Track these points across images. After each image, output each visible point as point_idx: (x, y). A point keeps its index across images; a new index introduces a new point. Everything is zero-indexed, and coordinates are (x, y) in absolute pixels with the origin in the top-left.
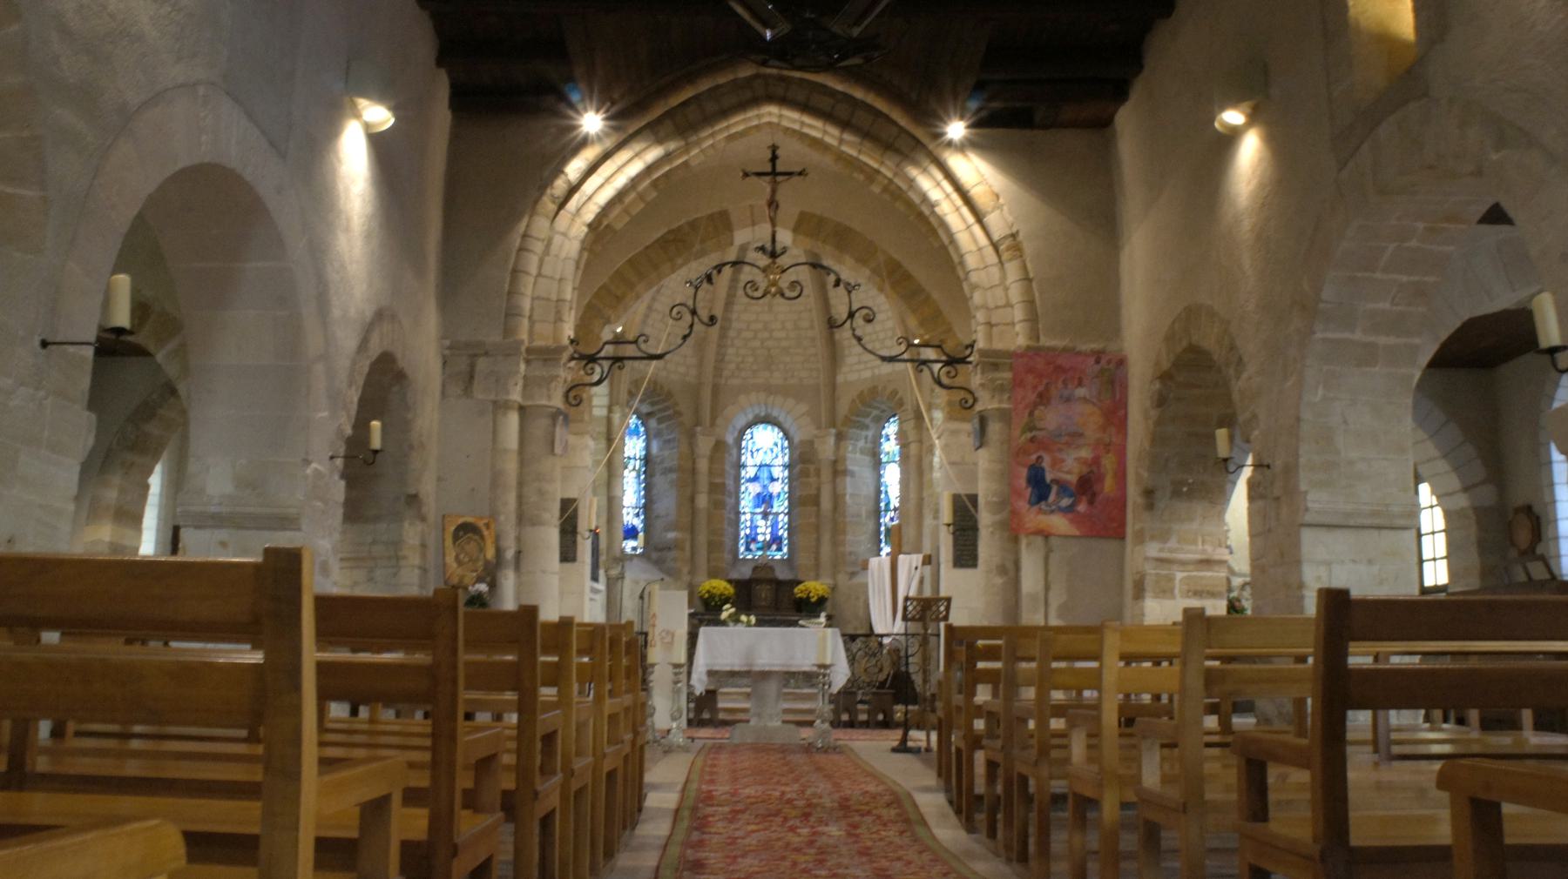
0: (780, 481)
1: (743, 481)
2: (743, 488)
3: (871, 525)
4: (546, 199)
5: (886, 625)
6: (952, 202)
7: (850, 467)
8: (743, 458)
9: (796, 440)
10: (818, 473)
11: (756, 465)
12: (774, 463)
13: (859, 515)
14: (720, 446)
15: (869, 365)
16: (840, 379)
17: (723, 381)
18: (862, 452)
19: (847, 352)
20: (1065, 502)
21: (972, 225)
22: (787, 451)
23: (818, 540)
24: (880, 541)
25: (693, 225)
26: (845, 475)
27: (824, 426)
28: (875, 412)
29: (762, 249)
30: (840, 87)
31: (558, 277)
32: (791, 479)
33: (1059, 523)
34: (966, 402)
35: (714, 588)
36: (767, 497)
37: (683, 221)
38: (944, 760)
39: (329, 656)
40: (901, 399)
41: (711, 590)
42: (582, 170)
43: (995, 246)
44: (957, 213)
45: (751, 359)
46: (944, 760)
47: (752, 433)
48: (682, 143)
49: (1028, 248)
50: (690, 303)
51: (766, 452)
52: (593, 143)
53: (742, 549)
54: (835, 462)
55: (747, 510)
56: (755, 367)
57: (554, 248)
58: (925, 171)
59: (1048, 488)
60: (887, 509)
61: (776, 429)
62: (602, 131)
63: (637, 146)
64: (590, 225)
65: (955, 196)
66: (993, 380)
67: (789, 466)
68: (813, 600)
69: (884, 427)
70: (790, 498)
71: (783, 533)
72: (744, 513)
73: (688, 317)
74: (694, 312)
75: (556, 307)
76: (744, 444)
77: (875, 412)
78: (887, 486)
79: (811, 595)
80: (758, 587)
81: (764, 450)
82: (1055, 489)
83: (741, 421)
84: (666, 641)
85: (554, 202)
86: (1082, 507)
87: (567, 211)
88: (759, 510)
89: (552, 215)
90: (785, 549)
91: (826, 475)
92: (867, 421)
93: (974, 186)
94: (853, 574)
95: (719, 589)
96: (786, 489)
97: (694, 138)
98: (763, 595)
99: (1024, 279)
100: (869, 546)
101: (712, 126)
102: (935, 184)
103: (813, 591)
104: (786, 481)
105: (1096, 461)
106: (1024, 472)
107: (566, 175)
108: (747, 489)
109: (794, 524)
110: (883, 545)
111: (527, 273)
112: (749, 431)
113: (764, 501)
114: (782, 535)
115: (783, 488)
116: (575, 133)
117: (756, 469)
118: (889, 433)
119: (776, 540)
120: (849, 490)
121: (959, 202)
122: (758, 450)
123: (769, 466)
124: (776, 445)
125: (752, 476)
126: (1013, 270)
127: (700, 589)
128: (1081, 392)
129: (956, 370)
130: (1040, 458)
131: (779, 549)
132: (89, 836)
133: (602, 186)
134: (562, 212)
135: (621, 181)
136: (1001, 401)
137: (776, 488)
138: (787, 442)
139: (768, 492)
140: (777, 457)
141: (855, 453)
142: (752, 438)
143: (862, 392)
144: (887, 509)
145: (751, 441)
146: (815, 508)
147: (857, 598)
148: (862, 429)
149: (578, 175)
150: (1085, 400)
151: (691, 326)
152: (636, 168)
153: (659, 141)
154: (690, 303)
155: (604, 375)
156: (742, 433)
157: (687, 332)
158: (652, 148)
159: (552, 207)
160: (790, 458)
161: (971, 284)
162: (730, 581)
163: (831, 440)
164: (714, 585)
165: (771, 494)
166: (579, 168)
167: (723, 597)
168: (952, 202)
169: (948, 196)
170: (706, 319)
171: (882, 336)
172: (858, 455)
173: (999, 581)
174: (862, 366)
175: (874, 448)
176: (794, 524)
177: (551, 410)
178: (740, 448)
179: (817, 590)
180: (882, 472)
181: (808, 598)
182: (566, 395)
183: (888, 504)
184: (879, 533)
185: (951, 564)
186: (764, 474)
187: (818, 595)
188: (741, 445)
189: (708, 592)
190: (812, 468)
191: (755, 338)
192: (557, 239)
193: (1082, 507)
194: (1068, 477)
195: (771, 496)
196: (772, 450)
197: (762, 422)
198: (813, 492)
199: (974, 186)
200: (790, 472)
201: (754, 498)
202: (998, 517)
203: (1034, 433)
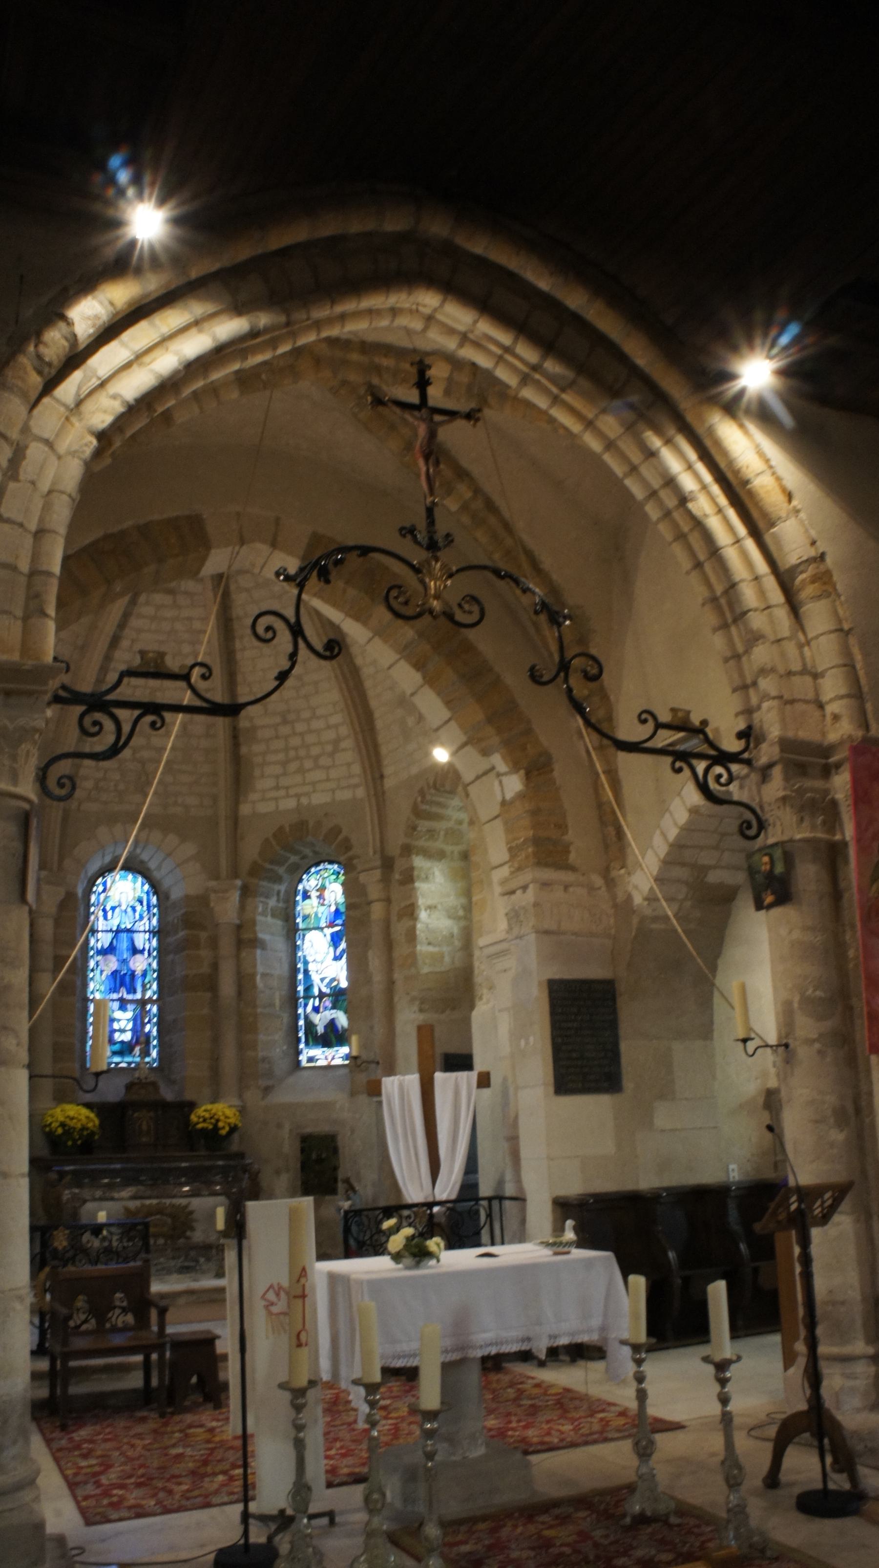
0: (146, 953)
1: (91, 953)
2: (92, 964)
3: (286, 1018)
4: (25, 361)
5: (422, 1186)
6: (713, 499)
7: (261, 935)
9: (176, 894)
10: (214, 943)
11: (111, 931)
12: (136, 928)
13: (272, 1005)
14: (70, 896)
15: (292, 792)
16: (245, 809)
18: (273, 916)
19: (257, 772)
21: (743, 539)
22: (155, 910)
23: (216, 1040)
24: (298, 1040)
25: (144, 530)
26: (255, 947)
27: (224, 873)
28: (293, 859)
29: (409, 532)
30: (544, 284)
31: (33, 526)
32: (162, 952)
35: (72, 1119)
36: (127, 979)
37: (128, 523)
40: (347, 840)
41: (68, 1122)
42: (99, 323)
44: (719, 516)
45: (117, 776)
47: (105, 884)
48: (282, 319)
49: (841, 581)
50: (290, 614)
51: (126, 911)
52: (138, 271)
54: (239, 927)
56: (121, 787)
57: (27, 469)
58: (668, 442)
60: (308, 995)
61: (140, 879)
62: (167, 249)
63: (197, 308)
64: (103, 436)
65: (716, 489)
66: (801, 792)
67: (158, 932)
68: (223, 1132)
69: (300, 880)
70: (159, 979)
71: (151, 1029)
73: (284, 638)
74: (297, 631)
75: (29, 586)
76: (93, 898)
77: (293, 859)
78: (306, 963)
79: (221, 1124)
80: (136, 1115)
81: (124, 907)
83: (94, 866)
84: (275, 1309)
85: (40, 373)
87: (58, 401)
88: (115, 996)
89: (34, 396)
90: (154, 1053)
91: (226, 945)
92: (281, 870)
93: (758, 475)
94: (267, 1090)
95: (79, 1120)
96: (155, 965)
97: (299, 315)
98: (144, 1127)
99: (836, 630)
100: (285, 1047)
101: (333, 303)
103: (222, 1118)
104: (155, 953)
107: (70, 323)
108: (97, 964)
109: (170, 1018)
110: (302, 1046)
111: (343, 326)
112: (100, 880)
113: (122, 984)
114: (150, 1032)
115: (150, 965)
116: (111, 235)
117: (110, 936)
118: (308, 888)
119: (141, 1040)
120: (260, 969)
121: (723, 500)
122: (113, 909)
123: (129, 931)
124: (140, 901)
125: (106, 945)
127: (50, 1120)
131: (146, 1053)
133: (127, 366)
134: (46, 400)
136: (813, 827)
137: (139, 964)
138: (155, 898)
139: (129, 969)
140: (141, 918)
141: (266, 916)
143: (281, 829)
144: (308, 995)
146: (208, 995)
147: (279, 1126)
148: (275, 882)
149: (91, 331)
151: (293, 657)
153: (238, 309)
154: (290, 614)
155: (121, 743)
156: (92, 883)
157: (285, 664)
158: (223, 317)
159: (35, 381)
160: (159, 921)
161: (751, 631)
162: (88, 1106)
163: (235, 896)
164: (72, 1113)
165: (133, 972)
166: (97, 317)
167: (85, 1133)
168: (713, 499)
170: (319, 646)
171: (315, 751)
172: (269, 919)
173: (838, 1136)
174: (282, 793)
175: (286, 909)
176: (170, 1018)
177: (14, 803)
178: (88, 906)
179: (227, 1117)
180: (299, 943)
181: (216, 1128)
182: (42, 778)
183: (308, 989)
184: (296, 1029)
185: (551, 1089)
186: (123, 944)
187: (229, 1124)
188: (89, 900)
189: (63, 1125)
190: (203, 935)
192: (35, 451)
195: (133, 974)
196: (134, 909)
198: (205, 969)
199: (758, 475)
200: (159, 941)
201: (107, 976)
202: (827, 1025)
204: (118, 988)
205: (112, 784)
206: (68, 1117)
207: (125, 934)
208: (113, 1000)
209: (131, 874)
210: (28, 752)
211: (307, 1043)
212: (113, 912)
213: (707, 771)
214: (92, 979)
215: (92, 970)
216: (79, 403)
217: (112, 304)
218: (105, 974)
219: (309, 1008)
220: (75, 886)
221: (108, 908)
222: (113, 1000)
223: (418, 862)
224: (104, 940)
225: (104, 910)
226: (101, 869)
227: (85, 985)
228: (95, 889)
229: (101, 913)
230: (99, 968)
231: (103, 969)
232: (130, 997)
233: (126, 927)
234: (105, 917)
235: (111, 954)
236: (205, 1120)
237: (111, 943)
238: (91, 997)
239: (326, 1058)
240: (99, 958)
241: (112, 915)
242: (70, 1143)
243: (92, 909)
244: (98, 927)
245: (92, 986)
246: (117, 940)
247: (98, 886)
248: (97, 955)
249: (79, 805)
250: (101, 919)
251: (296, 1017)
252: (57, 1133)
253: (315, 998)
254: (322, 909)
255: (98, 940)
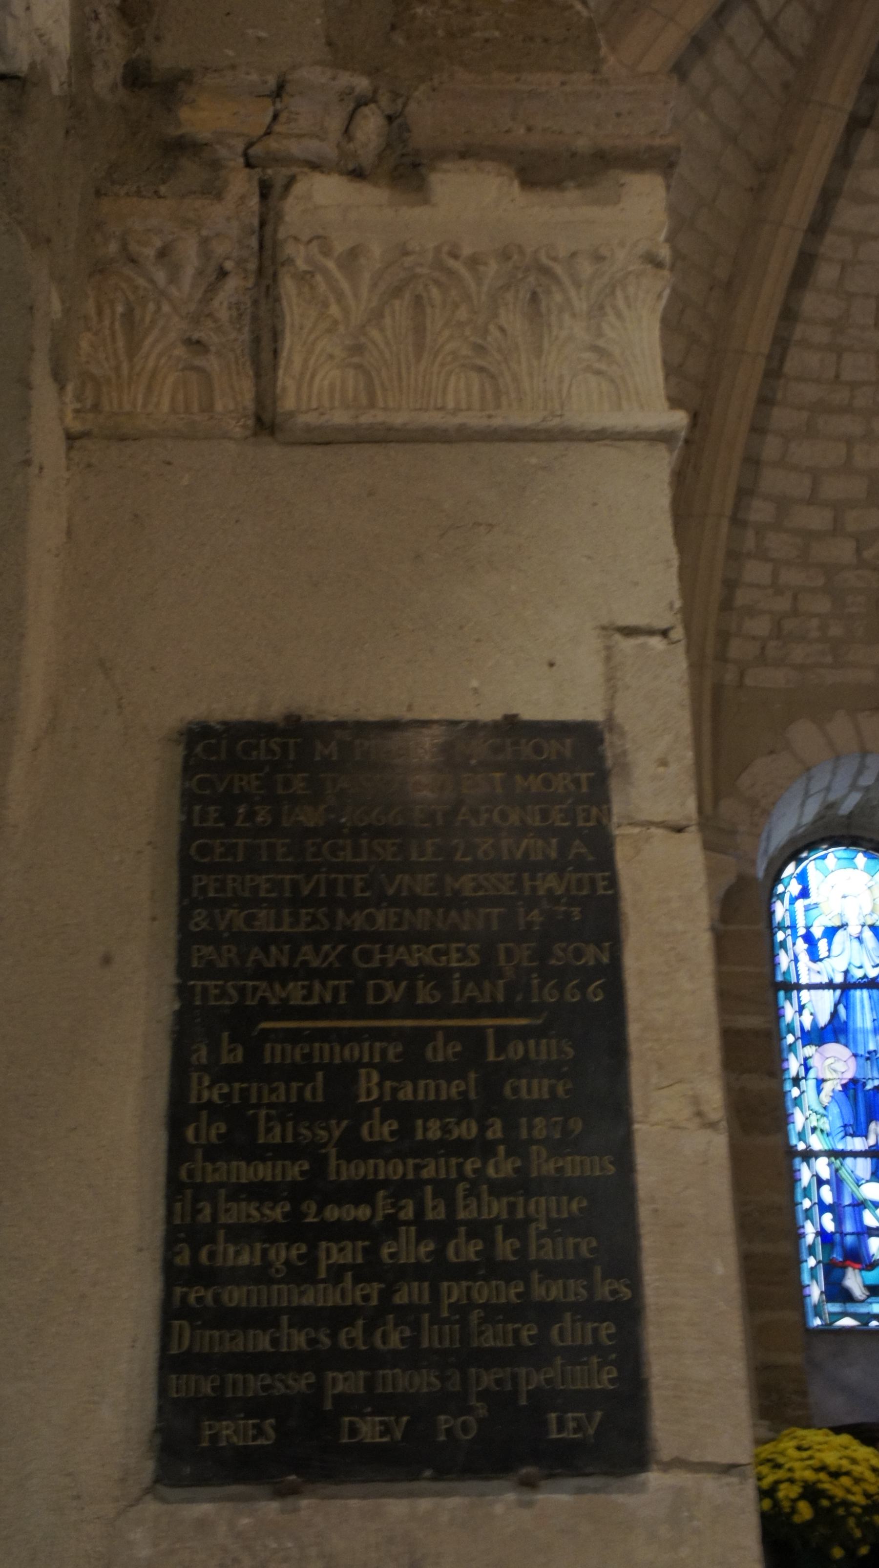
1: (790, 1039)
2: (794, 1066)
8: (784, 960)
17: (730, 677)
35: (836, 1475)
38: (857, 1219)
39: (490, 1031)
46: (857, 1219)
47: (802, 878)
53: (815, 1292)
55: (816, 1143)
56: (836, 631)
72: (809, 1155)
122: (830, 932)
125: (823, 1019)
142: (805, 893)
145: (800, 904)
164: (831, 1458)
189: (811, 1493)
191: (837, 530)
197: (835, 841)
204: (863, 1126)
205: (814, 622)
206: (823, 1468)
207: (865, 993)
208: (855, 1154)
209: (861, 855)
210: (334, 1379)
212: (830, 944)
214: (797, 1101)
215: (796, 1081)
218: (827, 1087)
220: (753, 863)
221: (817, 932)
222: (855, 1154)
225: (808, 938)
226: (792, 841)
227: (785, 1119)
228: (780, 889)
229: (801, 946)
230: (812, 1074)
231: (821, 1076)
233: (865, 976)
234: (814, 956)
235: (837, 1041)
237: (834, 1014)
238: (801, 1146)
240: (809, 1050)
241: (829, 950)
242: (838, 1553)
243: (780, 936)
244: (798, 975)
245: (799, 1119)
246: (846, 1007)
248: (804, 1046)
249: (742, 675)
250: (804, 958)
252: (797, 1519)
255: (801, 1008)
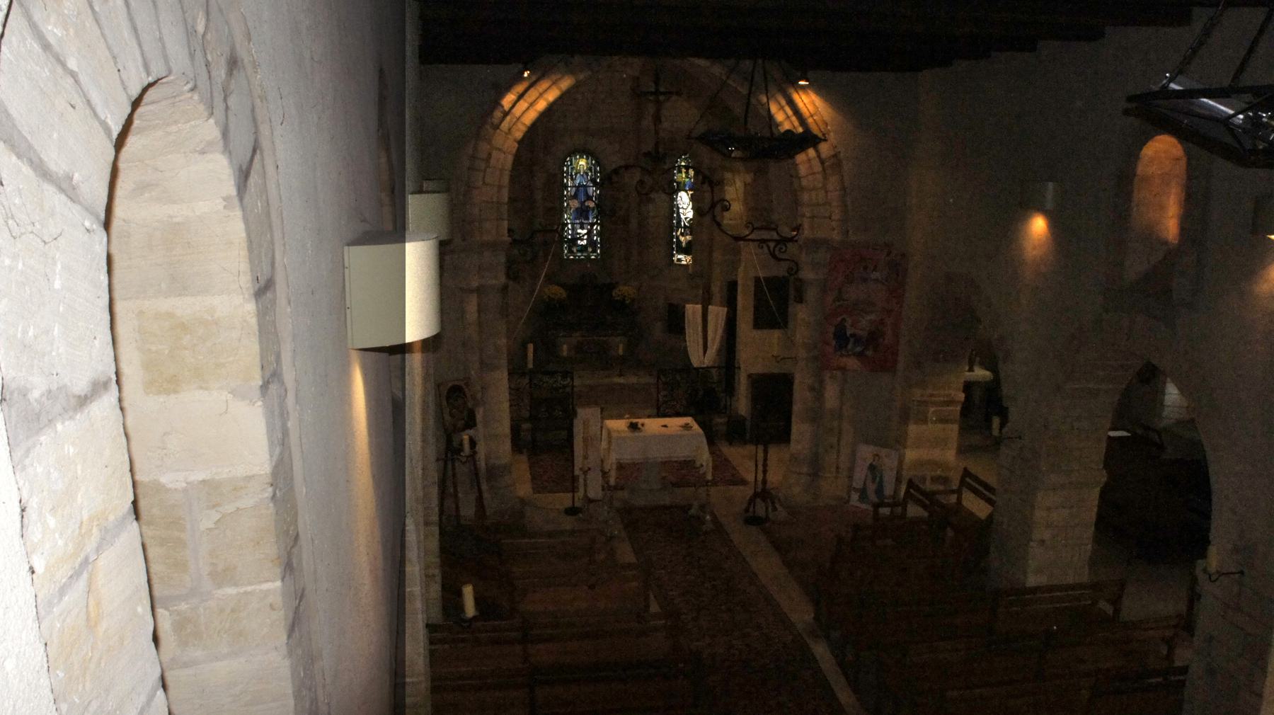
20: (859, 349)
33: (852, 363)
34: (792, 269)
43: (822, 162)
59: (847, 340)
78: (678, 208)
79: (626, 299)
82: (852, 340)
86: (869, 353)
102: (779, 107)
105: (882, 322)
106: (832, 329)
107: (503, 107)
108: (568, 205)
126: (833, 182)
128: (876, 275)
129: (786, 247)
130: (844, 320)
131: (594, 251)
132: (408, 625)
135: (541, 105)
150: (876, 280)
152: (552, 96)
162: (562, 286)
169: (788, 117)
193: (869, 353)
194: (860, 332)
201: (573, 211)
203: (842, 302)
211: (677, 252)
213: (775, 247)
216: (510, 129)
217: (518, 93)
219: (679, 233)
223: (728, 175)
224: (571, 191)
232: (586, 222)
236: (619, 295)
239: (686, 261)
247: (567, 162)
251: (673, 237)
253: (681, 228)
254: (687, 180)
